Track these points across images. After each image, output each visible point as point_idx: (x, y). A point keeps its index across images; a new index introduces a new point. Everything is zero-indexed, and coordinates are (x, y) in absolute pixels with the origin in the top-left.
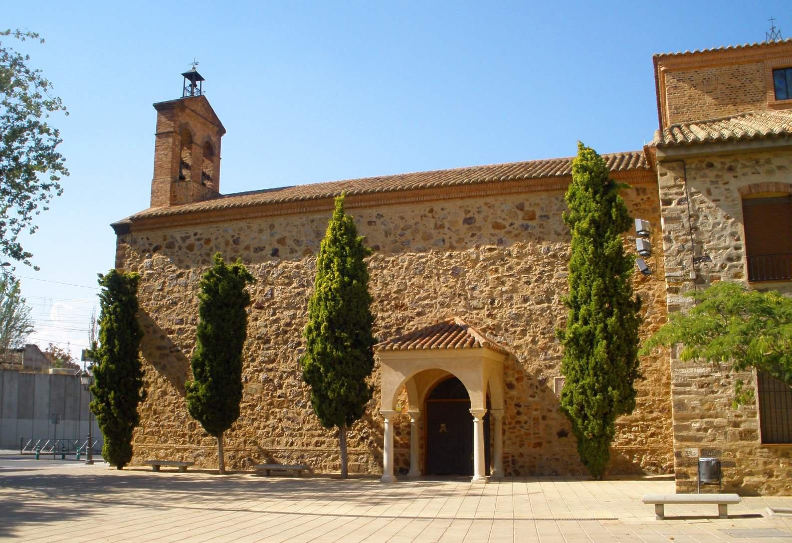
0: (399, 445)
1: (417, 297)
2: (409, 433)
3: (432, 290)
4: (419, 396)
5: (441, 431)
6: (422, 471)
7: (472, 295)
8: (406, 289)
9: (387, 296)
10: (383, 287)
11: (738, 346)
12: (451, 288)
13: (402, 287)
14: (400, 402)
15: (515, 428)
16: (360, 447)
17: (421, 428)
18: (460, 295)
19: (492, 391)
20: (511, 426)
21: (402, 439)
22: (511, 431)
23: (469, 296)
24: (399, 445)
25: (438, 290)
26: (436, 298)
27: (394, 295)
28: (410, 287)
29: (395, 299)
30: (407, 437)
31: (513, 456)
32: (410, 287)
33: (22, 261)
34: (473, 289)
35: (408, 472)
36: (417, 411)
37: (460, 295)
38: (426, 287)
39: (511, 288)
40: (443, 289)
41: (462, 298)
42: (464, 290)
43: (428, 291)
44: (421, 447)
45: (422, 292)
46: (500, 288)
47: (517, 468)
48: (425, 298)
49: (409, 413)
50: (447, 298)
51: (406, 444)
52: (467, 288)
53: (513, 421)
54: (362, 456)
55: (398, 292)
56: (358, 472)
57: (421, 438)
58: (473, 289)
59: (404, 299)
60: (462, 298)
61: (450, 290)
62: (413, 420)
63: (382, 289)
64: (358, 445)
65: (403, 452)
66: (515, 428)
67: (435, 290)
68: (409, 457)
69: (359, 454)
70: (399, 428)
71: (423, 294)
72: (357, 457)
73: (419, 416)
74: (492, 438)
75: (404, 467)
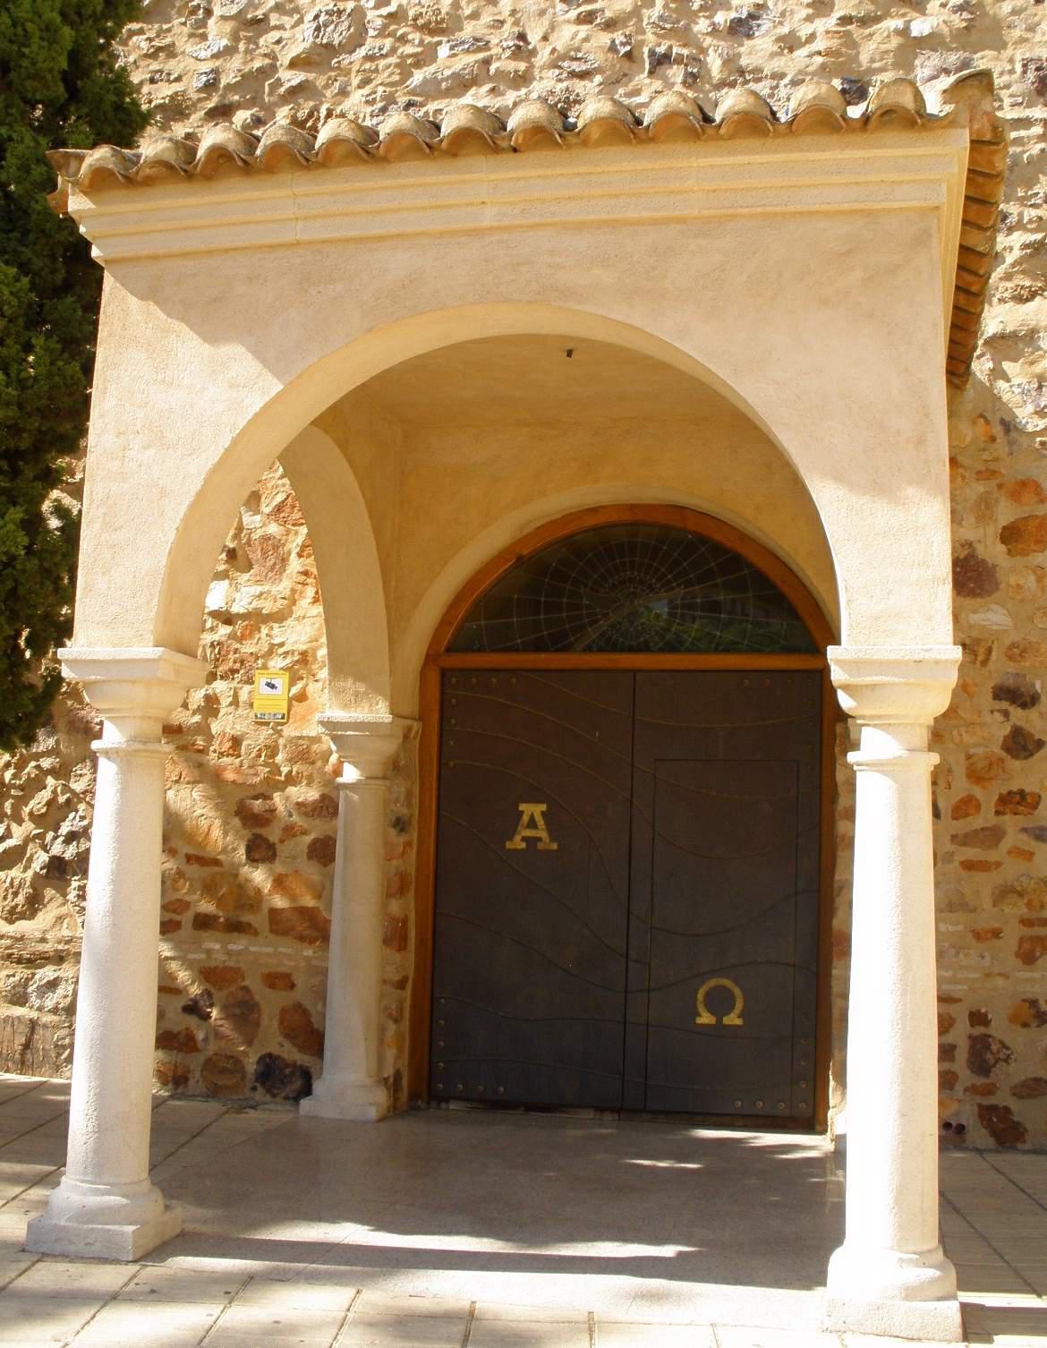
0: (259, 920)
1: (418, 77)
2: (323, 851)
3: (502, 40)
4: (397, 617)
5: (517, 843)
6: (393, 1085)
7: (730, 62)
8: (356, 41)
9: (252, 82)
10: (235, 38)
11: (1018, 803)
12: (610, 25)
13: (336, 35)
14: (277, 663)
15: (993, 836)
16: (44, 918)
17: (400, 824)
18: (660, 62)
19: (940, 1295)
20: (977, 822)
21: (279, 883)
22: (971, 853)
23: (714, 64)
24: (187, 918)
25: (534, 38)
26: (522, 79)
27: (291, 78)
28: (382, 33)
29: (295, 92)
30: (312, 871)
31: (978, 1018)
32: (382, 33)
33: (289, 622)
34: (741, 28)
35: (307, 1091)
36: (379, 712)
37: (660, 62)
38: (469, 30)
39: (958, 21)
40: (567, 35)
41: (676, 73)
42: (685, 36)
43: (479, 44)
44: (394, 936)
45: (443, 51)
46: (898, 23)
47: (1003, 1098)
48: (462, 84)
49: (330, 725)
50: (584, 75)
51: (303, 912)
52: (702, 25)
53: (987, 797)
54: (48, 973)
55: (318, 57)
56: (23, 1065)
57: (396, 886)
58: (741, 28)
59: (343, 93)
60: (676, 73)
61: (605, 38)
62: (350, 774)
63: (229, 51)
64: (34, 904)
65: (286, 966)
66: (993, 836)
67: (522, 37)
68: (321, 994)
69: (34, 962)
70: (267, 818)
71: (449, 61)
72: (22, 972)
73: (389, 747)
74: (510, 1324)
75: (291, 1054)
